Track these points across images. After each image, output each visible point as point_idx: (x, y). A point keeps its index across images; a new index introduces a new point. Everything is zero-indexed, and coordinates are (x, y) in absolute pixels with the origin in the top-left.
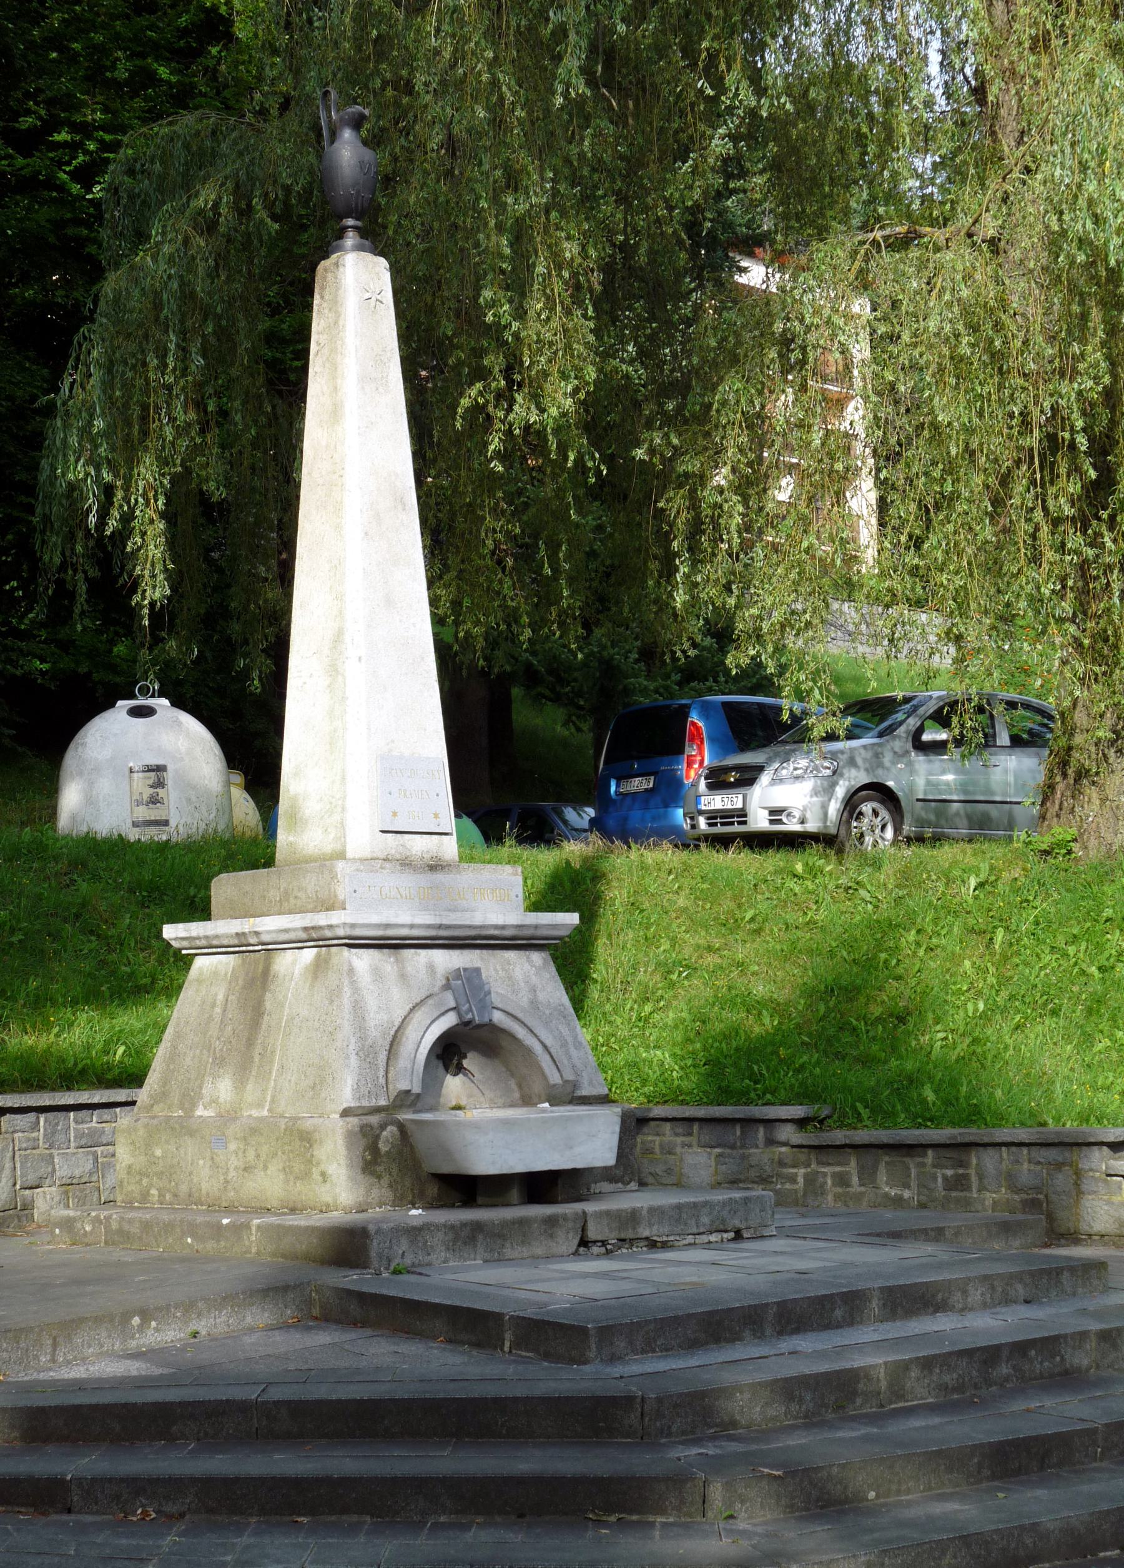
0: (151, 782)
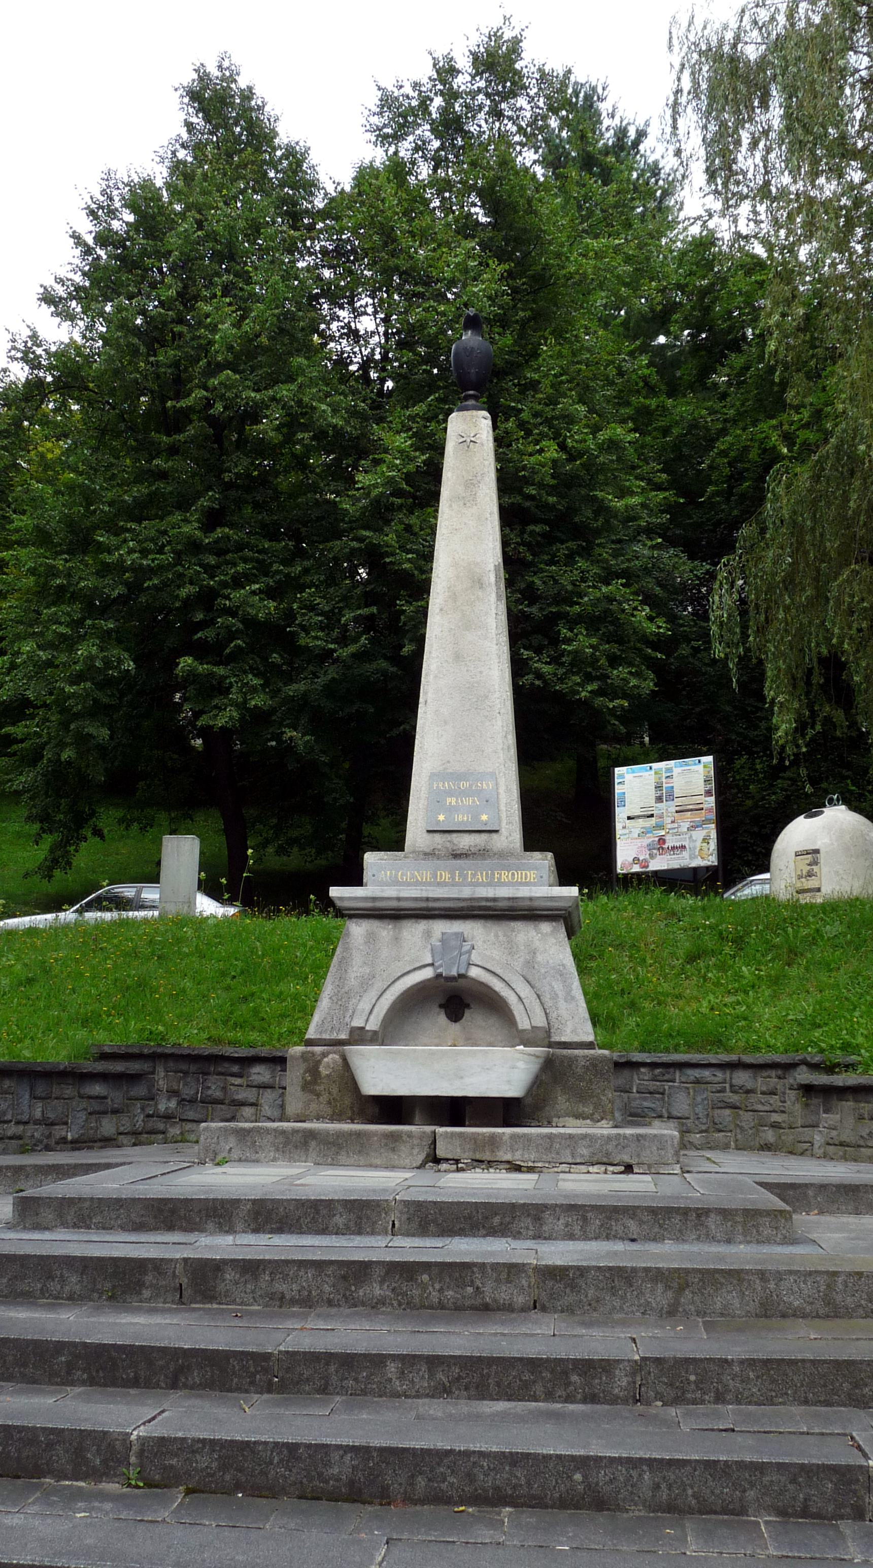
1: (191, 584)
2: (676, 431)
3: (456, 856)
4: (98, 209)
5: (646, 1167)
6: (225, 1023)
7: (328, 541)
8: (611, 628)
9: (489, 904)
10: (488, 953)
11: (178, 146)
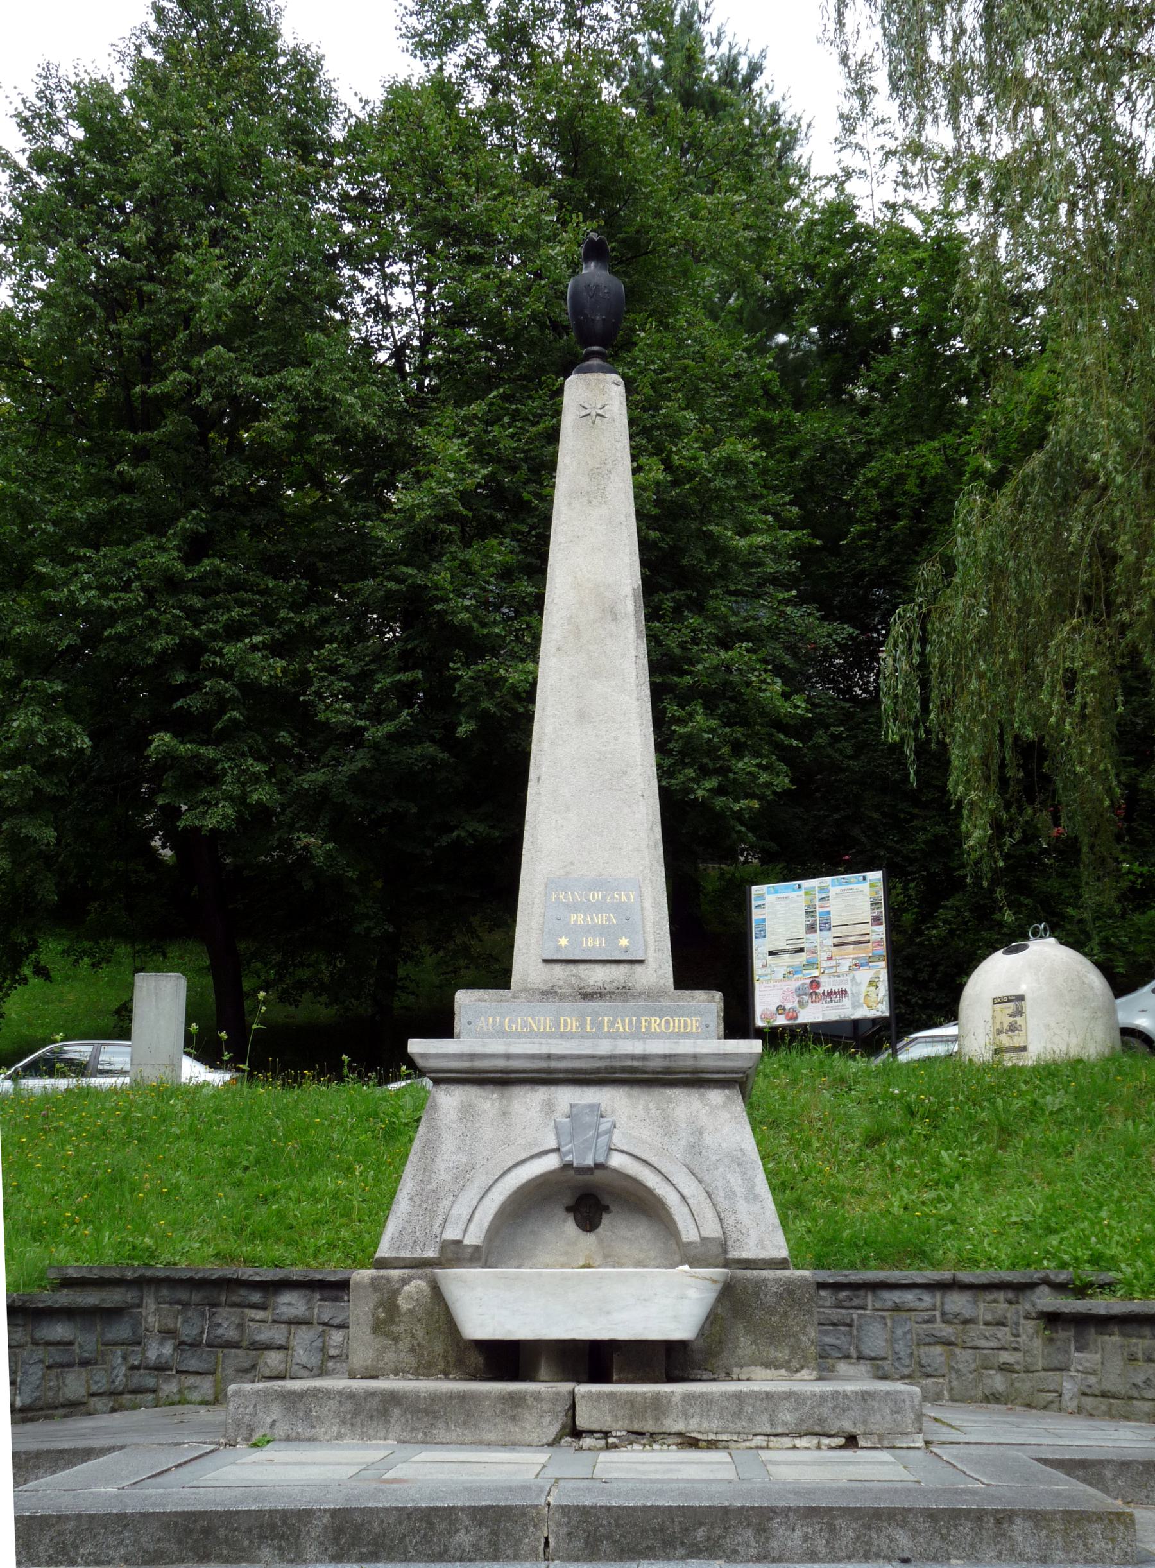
0: (1010, 1011)
1: (168, 633)
2: (806, 454)
4: (34, 118)
5: (875, 1438)
6: (239, 1232)
7: (354, 581)
8: (732, 706)
9: (636, 1064)
11: (144, 39)
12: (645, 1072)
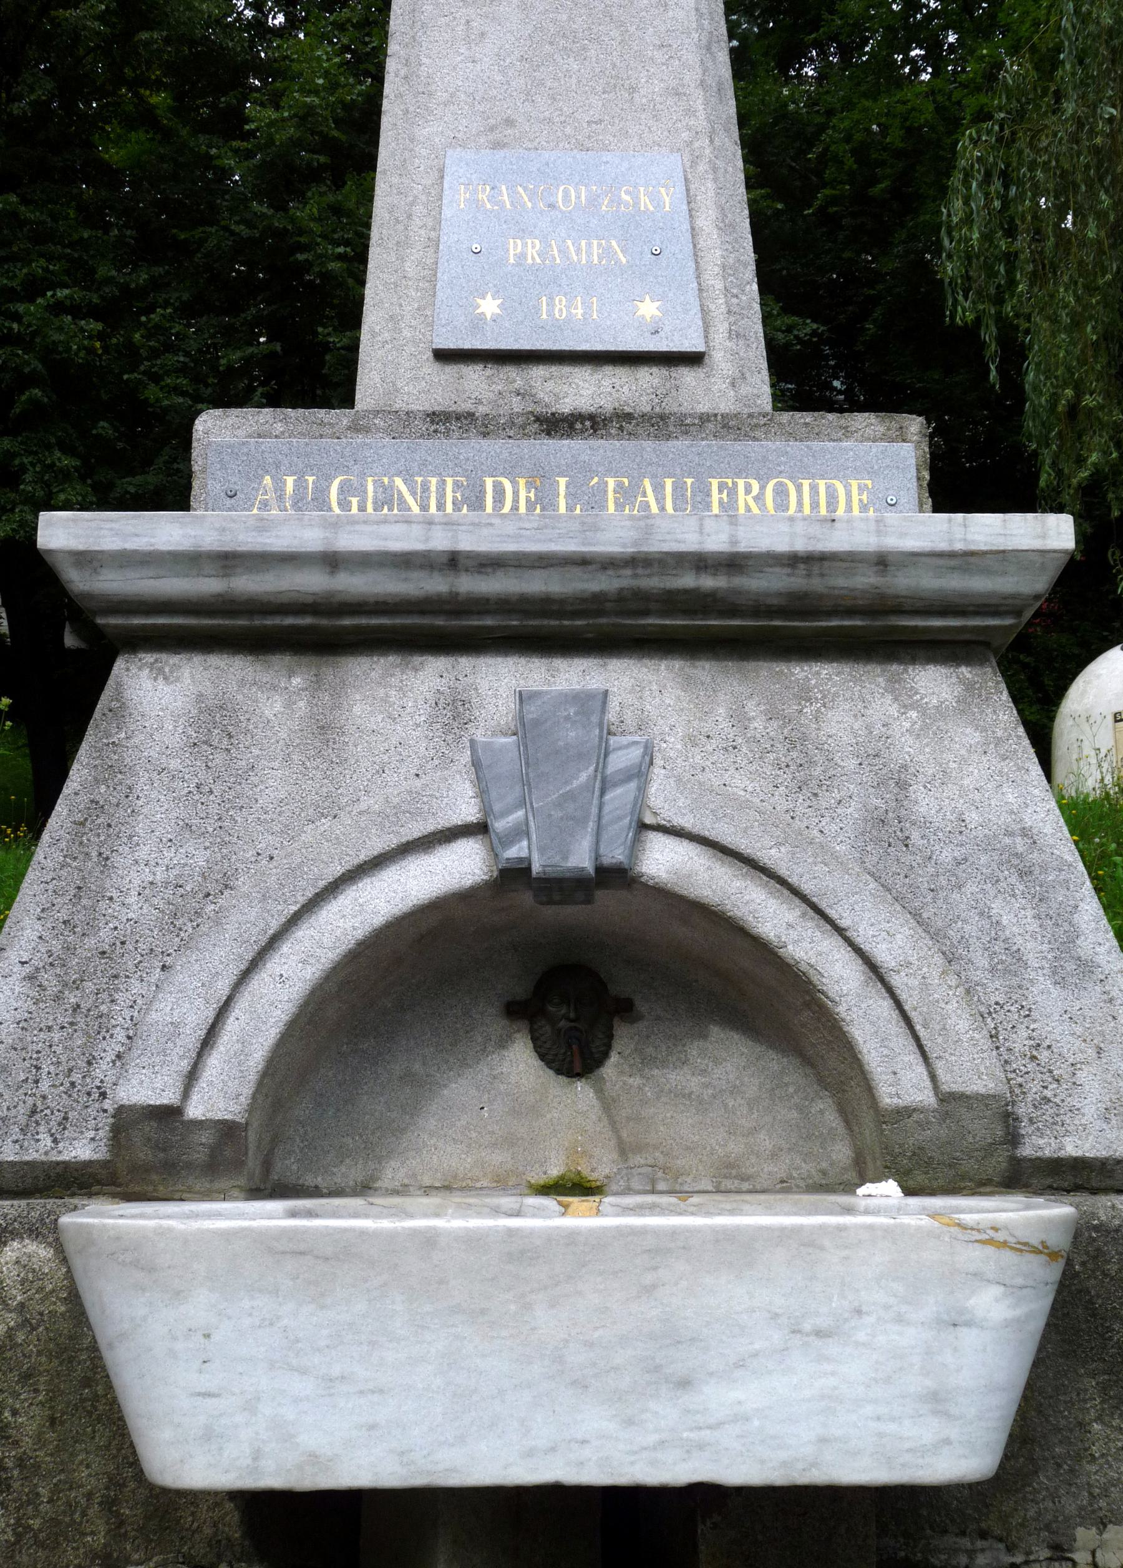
3: (556, 425)
9: (708, 582)
10: (713, 779)
12: (733, 611)
